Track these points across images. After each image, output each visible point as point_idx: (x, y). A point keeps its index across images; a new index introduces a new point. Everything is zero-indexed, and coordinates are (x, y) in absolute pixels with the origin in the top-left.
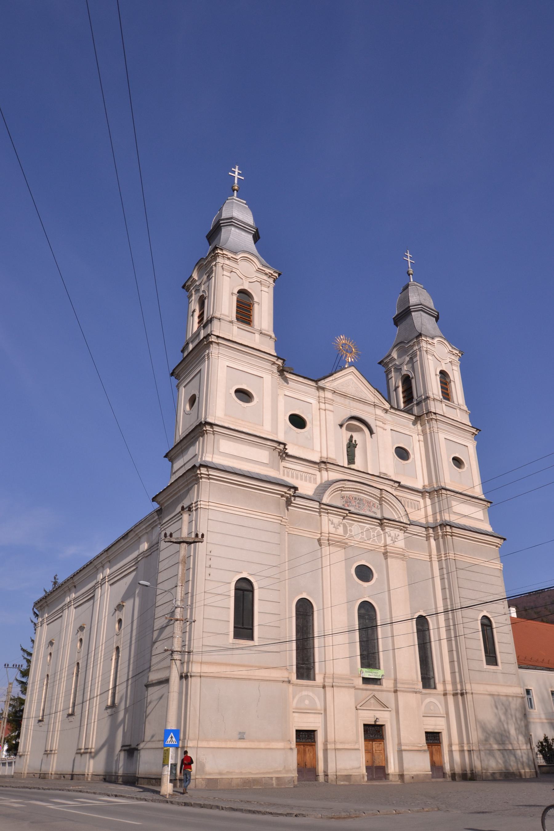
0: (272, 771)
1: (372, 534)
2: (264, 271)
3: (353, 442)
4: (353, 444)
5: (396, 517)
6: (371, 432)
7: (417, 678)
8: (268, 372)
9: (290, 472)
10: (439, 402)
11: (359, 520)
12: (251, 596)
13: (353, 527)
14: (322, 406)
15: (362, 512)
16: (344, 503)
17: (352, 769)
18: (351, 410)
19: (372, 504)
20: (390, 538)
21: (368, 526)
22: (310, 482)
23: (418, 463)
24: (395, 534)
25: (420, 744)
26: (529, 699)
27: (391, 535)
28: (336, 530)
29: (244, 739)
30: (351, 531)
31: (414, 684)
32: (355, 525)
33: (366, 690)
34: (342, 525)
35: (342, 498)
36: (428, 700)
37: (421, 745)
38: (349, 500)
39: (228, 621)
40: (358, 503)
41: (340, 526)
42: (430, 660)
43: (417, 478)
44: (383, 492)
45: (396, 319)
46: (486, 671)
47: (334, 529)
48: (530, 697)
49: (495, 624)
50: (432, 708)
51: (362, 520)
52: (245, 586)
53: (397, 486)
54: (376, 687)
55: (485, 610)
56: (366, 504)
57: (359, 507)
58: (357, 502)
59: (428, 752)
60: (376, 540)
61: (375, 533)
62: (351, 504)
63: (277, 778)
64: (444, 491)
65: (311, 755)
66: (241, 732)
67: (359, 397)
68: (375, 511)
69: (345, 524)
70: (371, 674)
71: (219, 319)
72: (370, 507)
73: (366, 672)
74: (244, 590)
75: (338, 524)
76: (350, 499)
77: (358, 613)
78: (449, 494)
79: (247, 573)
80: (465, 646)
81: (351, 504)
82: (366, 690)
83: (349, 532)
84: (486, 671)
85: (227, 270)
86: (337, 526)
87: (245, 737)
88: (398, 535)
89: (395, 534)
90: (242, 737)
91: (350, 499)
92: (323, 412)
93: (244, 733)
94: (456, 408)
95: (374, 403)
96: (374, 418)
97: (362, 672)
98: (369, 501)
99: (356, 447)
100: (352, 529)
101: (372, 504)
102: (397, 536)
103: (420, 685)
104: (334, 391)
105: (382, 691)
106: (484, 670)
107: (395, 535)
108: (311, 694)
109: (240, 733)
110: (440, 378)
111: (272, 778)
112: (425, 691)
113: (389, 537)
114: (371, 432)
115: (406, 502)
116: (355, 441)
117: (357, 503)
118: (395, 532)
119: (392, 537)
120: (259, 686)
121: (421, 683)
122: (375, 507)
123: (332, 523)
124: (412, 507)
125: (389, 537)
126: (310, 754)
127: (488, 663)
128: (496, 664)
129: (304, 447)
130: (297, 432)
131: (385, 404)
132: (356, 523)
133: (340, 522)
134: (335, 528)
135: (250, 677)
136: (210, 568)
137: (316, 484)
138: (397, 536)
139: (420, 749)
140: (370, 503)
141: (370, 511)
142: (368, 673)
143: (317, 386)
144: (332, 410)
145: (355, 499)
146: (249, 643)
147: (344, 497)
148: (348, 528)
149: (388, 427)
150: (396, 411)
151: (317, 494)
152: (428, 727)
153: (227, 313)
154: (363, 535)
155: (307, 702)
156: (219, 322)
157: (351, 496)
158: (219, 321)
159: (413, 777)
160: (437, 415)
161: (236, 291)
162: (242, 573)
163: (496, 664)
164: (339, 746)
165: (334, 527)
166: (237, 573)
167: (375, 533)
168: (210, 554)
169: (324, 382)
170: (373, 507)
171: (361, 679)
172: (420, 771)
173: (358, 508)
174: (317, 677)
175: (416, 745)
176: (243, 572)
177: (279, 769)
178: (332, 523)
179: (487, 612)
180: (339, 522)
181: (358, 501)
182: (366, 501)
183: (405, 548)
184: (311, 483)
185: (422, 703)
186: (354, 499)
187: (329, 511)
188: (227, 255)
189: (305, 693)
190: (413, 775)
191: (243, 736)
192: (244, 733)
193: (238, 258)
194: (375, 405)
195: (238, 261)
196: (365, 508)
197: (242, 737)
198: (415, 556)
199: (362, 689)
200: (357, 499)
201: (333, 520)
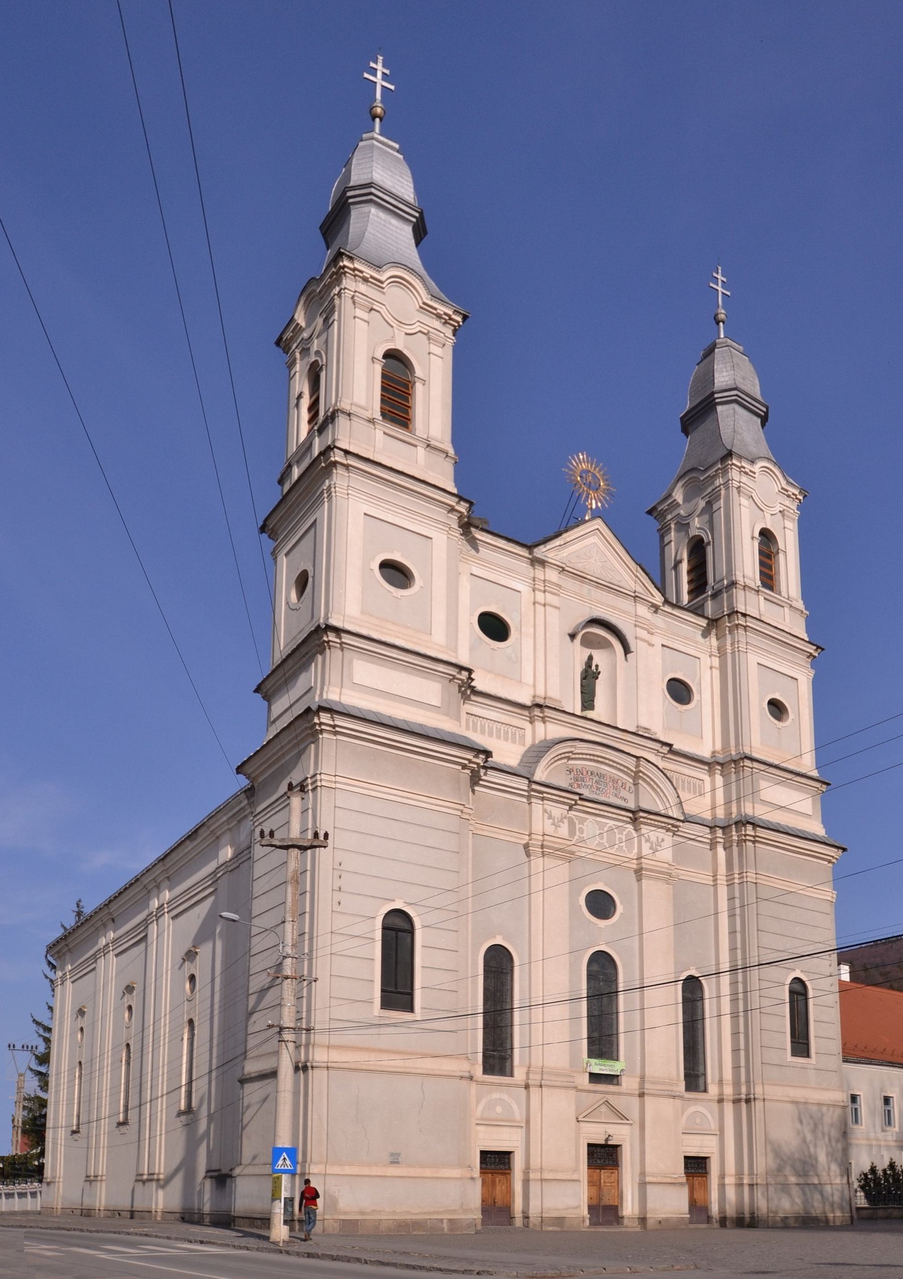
0: (442, 1210)
2: (435, 309)
3: (594, 668)
4: (593, 672)
5: (661, 808)
6: (627, 650)
7: (678, 1075)
8: (441, 527)
9: (479, 722)
10: (753, 592)
11: (597, 812)
12: (409, 940)
13: (585, 824)
14: (540, 597)
17: (567, 1209)
18: (592, 606)
19: (620, 783)
20: (648, 844)
21: (611, 823)
22: (514, 741)
23: (707, 710)
24: (658, 838)
25: (675, 1174)
28: (556, 829)
29: (398, 1163)
31: (672, 1085)
32: (588, 821)
33: (595, 1092)
34: (566, 821)
35: (568, 772)
36: (692, 1109)
37: (676, 1176)
38: (581, 775)
39: (372, 981)
40: (596, 781)
41: (563, 823)
42: (700, 1047)
43: (702, 738)
45: (685, 419)
46: (789, 1066)
50: (698, 1121)
51: (602, 813)
52: (399, 922)
53: (666, 752)
54: (611, 1088)
55: (798, 968)
56: (611, 784)
57: (597, 789)
58: (595, 779)
60: (624, 848)
61: (622, 835)
63: (450, 1221)
64: (747, 763)
65: (503, 1187)
66: (394, 1152)
67: (608, 580)
68: (625, 797)
70: (603, 1068)
71: (349, 415)
73: (596, 1064)
74: (397, 930)
76: (582, 774)
77: (588, 971)
78: (756, 767)
79: (403, 901)
81: (583, 783)
82: (595, 1092)
85: (362, 307)
86: (558, 822)
87: (400, 1160)
89: (658, 838)
90: (395, 1160)
91: (582, 774)
92: (540, 608)
93: (399, 1155)
94: (783, 604)
98: (616, 777)
99: (597, 678)
100: (584, 828)
101: (620, 783)
102: (660, 841)
104: (561, 567)
105: (620, 1094)
106: (787, 1064)
107: (658, 840)
108: (505, 1097)
109: (392, 1154)
110: (759, 544)
111: (442, 1220)
114: (627, 650)
115: (680, 781)
116: (597, 666)
117: (594, 781)
118: (658, 834)
119: (652, 844)
121: (684, 1082)
122: (625, 788)
123: (550, 817)
126: (501, 1186)
130: (492, 647)
132: (591, 818)
133: (563, 816)
134: (555, 825)
135: (408, 1070)
136: (339, 892)
137: (524, 745)
139: (674, 1181)
141: (616, 796)
142: (599, 1066)
143: (530, 557)
144: (558, 605)
145: (592, 774)
146: (407, 1016)
147: (573, 771)
148: (578, 826)
149: (657, 640)
150: (673, 609)
151: (525, 764)
152: (689, 1149)
153: (363, 402)
154: (602, 839)
155: (499, 1109)
156: (349, 421)
158: (348, 418)
159: (660, 1222)
160: (748, 618)
161: (379, 354)
162: (395, 901)
164: (547, 1176)
165: (553, 824)
166: (386, 901)
167: (622, 835)
168: (340, 868)
169: (544, 550)
171: (588, 1075)
173: (595, 790)
174: (516, 1072)
177: (453, 1208)
178: (550, 817)
179: (801, 971)
180: (562, 814)
181: (597, 778)
182: (610, 777)
183: (673, 862)
184: (515, 743)
185: (683, 1114)
186: (589, 774)
187: (545, 795)
188: (361, 272)
190: (660, 1219)
191: (397, 1159)
192: (399, 1155)
193: (383, 278)
194: (637, 596)
195: (384, 286)
196: (608, 791)
197: (395, 1160)
198: (688, 876)
199: (589, 1091)
200: (595, 774)
201: (550, 812)
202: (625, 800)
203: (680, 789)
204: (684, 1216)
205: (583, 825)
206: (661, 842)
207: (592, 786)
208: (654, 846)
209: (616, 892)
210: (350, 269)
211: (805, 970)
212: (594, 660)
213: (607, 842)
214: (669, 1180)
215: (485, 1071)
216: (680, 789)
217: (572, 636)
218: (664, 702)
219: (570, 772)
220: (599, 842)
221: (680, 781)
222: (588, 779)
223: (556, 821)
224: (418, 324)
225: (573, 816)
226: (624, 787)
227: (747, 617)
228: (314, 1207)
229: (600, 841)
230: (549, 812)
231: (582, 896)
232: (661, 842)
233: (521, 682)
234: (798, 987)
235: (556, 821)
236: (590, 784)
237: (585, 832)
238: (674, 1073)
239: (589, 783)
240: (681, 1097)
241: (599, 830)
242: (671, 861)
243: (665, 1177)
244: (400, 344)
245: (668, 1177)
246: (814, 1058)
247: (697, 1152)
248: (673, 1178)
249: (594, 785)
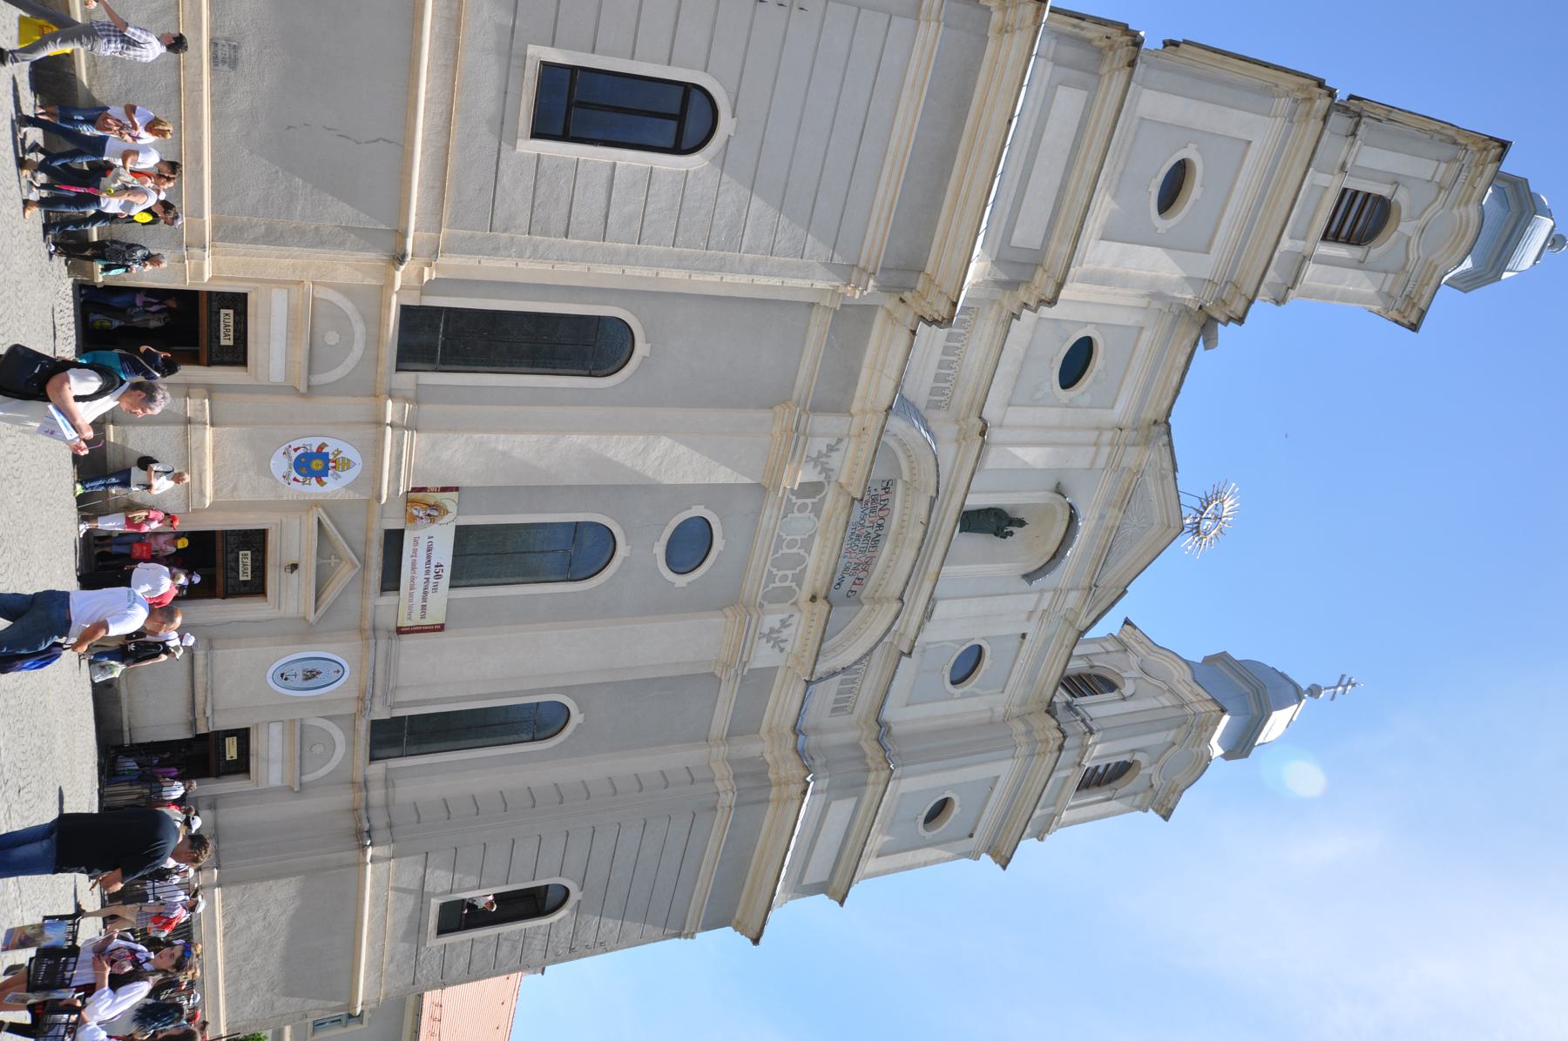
1: (789, 573)
3: (1010, 529)
6: (1029, 577)
12: (660, 143)
13: (812, 515)
14: (1107, 436)
15: (1262, 287)
16: (873, 493)
20: (777, 625)
23: (941, 708)
24: (786, 641)
26: (338, 1018)
27: (785, 627)
28: (812, 459)
30: (803, 508)
31: (385, 694)
32: (816, 519)
34: (821, 478)
36: (339, 736)
37: (209, 713)
38: (879, 507)
40: (869, 533)
43: (907, 705)
44: (895, 605)
45: (1224, 657)
46: (422, 902)
47: (815, 455)
48: (344, 1022)
49: (546, 926)
54: (375, 575)
57: (858, 536)
59: (189, 736)
61: (792, 581)
62: (867, 512)
69: (821, 492)
71: (1354, 134)
72: (854, 568)
74: (681, 118)
75: (828, 466)
76: (880, 509)
79: (732, 134)
80: (1024, 647)
81: (867, 512)
83: (800, 502)
84: (422, 902)
86: (822, 463)
88: (782, 650)
89: (786, 641)
92: (1093, 436)
95: (1096, 586)
96: (1060, 586)
97: (434, 513)
99: (996, 535)
102: (782, 645)
103: (381, 713)
110: (1125, 762)
112: (363, 728)
113: (781, 621)
114: (1029, 577)
115: (854, 676)
116: (1011, 533)
117: (869, 530)
120: (390, 142)
121: (388, 717)
122: (854, 583)
123: (831, 448)
124: (841, 694)
125: (781, 621)
127: (445, 908)
128: (443, 930)
129: (1018, 377)
130: (1055, 358)
131: (1090, 616)
133: (830, 473)
134: (818, 458)
137: (927, 408)
138: (782, 645)
139: (199, 708)
140: (864, 570)
141: (847, 568)
145: (880, 525)
146: (525, 118)
148: (809, 501)
154: (788, 547)
156: (1344, 133)
157: (886, 512)
158: (1349, 133)
162: (733, 117)
163: (443, 930)
165: (820, 454)
166: (733, 100)
167: (792, 581)
170: (852, 579)
172: (129, 710)
173: (857, 532)
175: (209, 699)
176: (735, 119)
178: (831, 448)
179: (579, 901)
180: (832, 470)
181: (873, 535)
182: (872, 558)
186: (880, 522)
189: (359, 329)
190: (116, 685)
193: (1470, 206)
194: (1091, 589)
200: (879, 532)
201: (838, 449)
202: (838, 584)
203: (844, 677)
204: (126, 735)
205: (810, 512)
206: (779, 647)
207: (862, 526)
208: (774, 635)
209: (706, 574)
210: (1485, 159)
211: (581, 905)
212: (1019, 529)
213: (783, 554)
214: (200, 698)
215: (548, 70)
216: (844, 677)
217: (1059, 490)
218: (955, 642)
219: (885, 489)
220: (784, 540)
221: (854, 676)
222: (873, 519)
223: (824, 460)
224: (1159, 784)
225: (824, 492)
226: (857, 582)
227: (1058, 753)
228: (59, 40)
229: (785, 543)
230: (837, 447)
231: (707, 511)
232: (779, 647)
233: (1009, 405)
234: (552, 898)
235: (824, 460)
236: (867, 524)
237: (803, 515)
238: (403, 696)
239: (867, 522)
240: (362, 711)
241: (802, 539)
242: (752, 667)
243: (206, 690)
244: (1404, 227)
245: (206, 697)
246: (435, 942)
247: (257, 754)
248: (205, 706)
249: (864, 531)
